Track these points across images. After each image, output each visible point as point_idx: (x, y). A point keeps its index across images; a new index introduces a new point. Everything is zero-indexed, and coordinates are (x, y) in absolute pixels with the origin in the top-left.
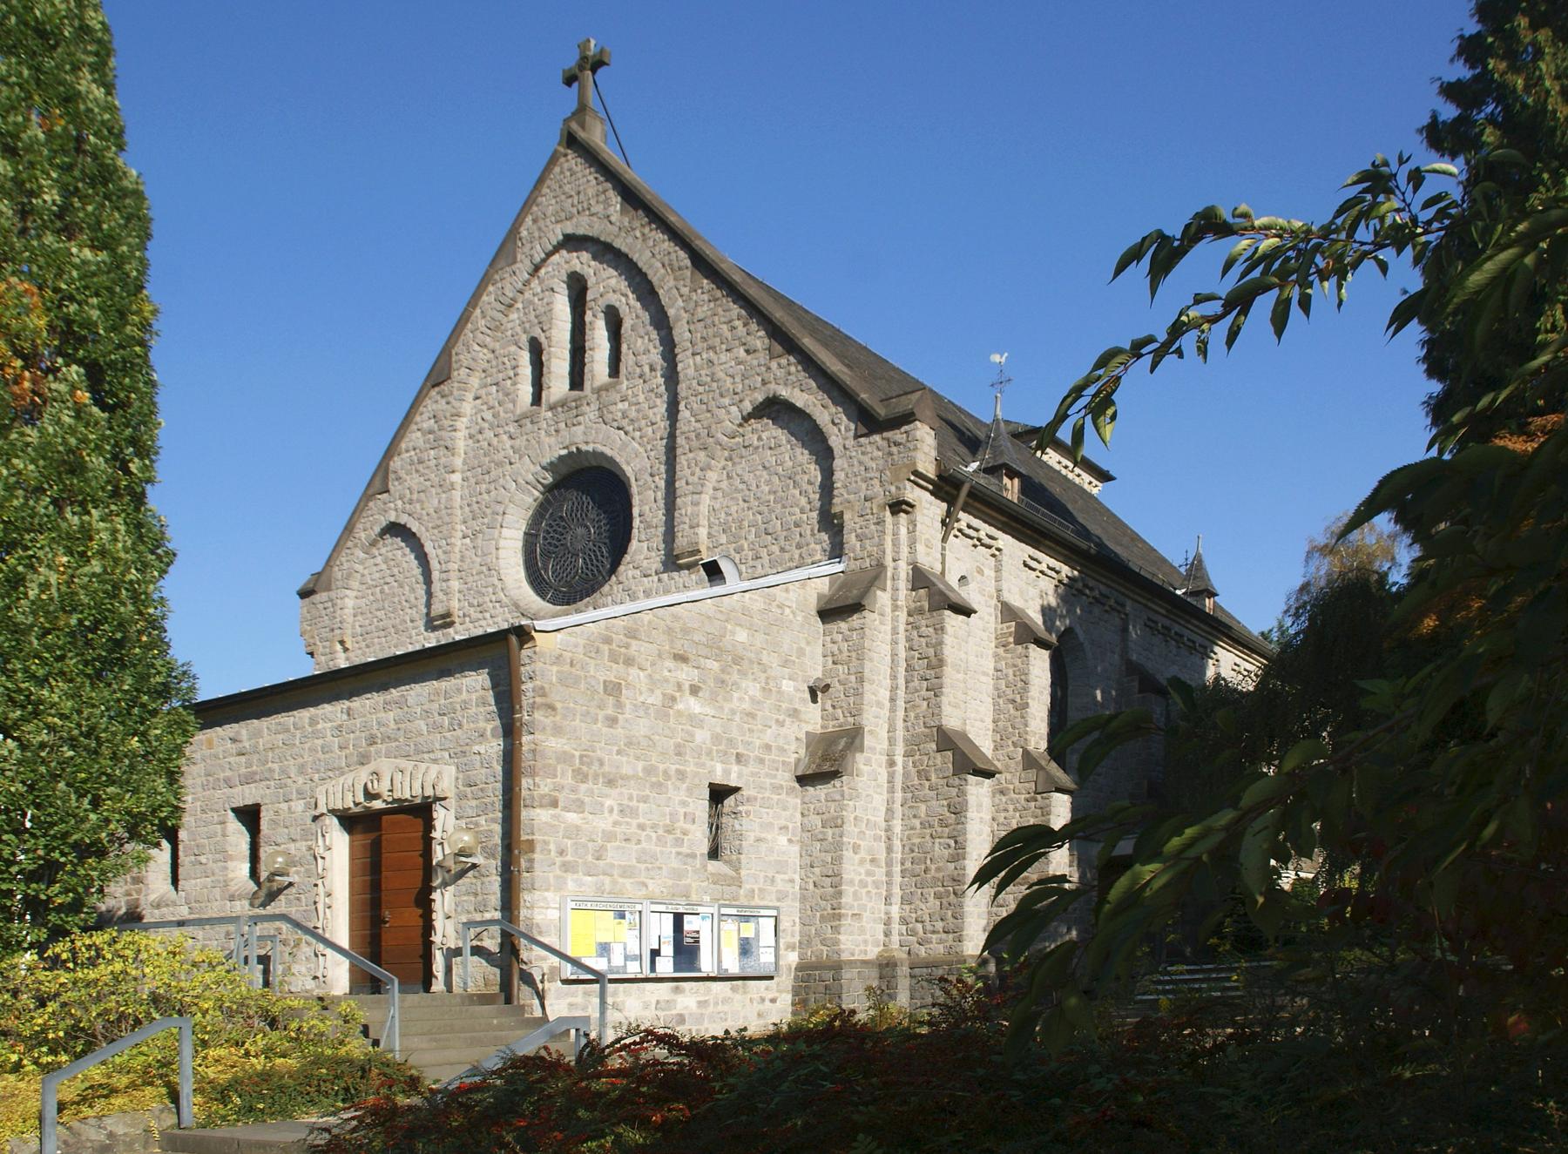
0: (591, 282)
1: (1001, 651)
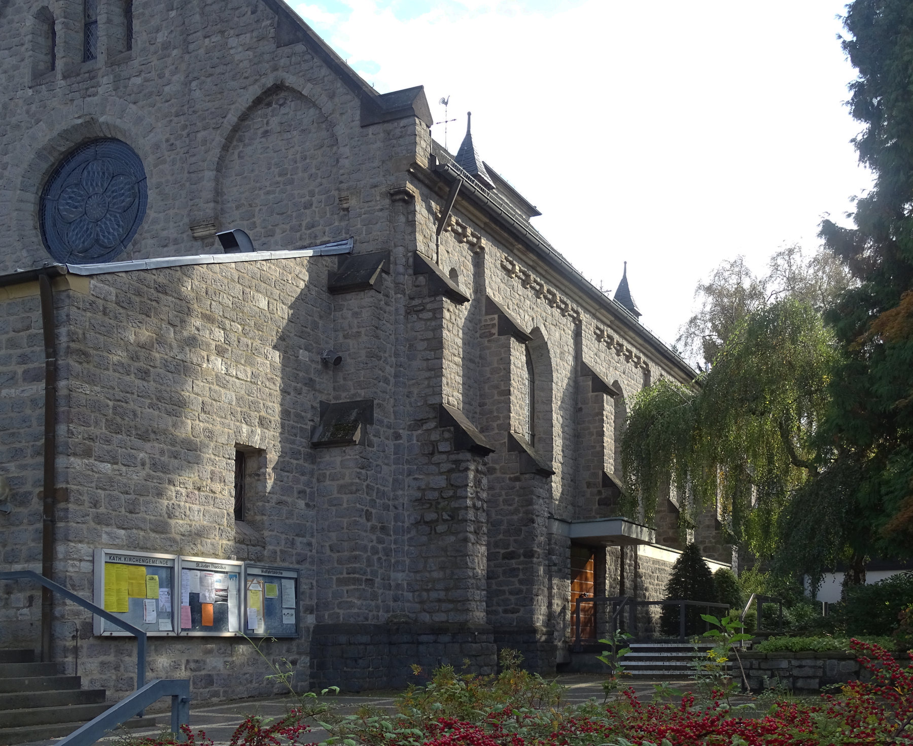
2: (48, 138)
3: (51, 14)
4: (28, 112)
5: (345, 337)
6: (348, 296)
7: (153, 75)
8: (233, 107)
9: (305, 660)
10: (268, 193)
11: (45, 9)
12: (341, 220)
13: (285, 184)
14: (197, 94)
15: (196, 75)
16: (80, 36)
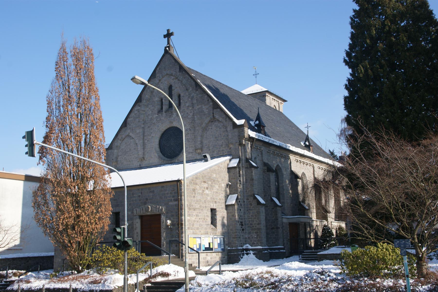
9: (226, 257)
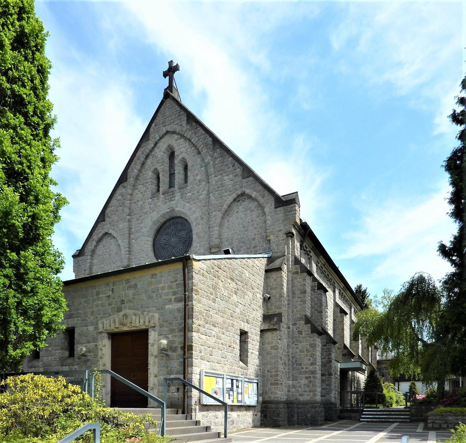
0: (176, 149)
1: (312, 292)
2: (157, 217)
3: (158, 171)
4: (150, 208)
5: (271, 289)
6: (272, 273)
7: (195, 192)
8: (226, 202)
9: (259, 414)
10: (239, 235)
11: (156, 169)
12: (266, 244)
13: (245, 231)
14: (212, 198)
15: (212, 191)
16: (168, 179)
